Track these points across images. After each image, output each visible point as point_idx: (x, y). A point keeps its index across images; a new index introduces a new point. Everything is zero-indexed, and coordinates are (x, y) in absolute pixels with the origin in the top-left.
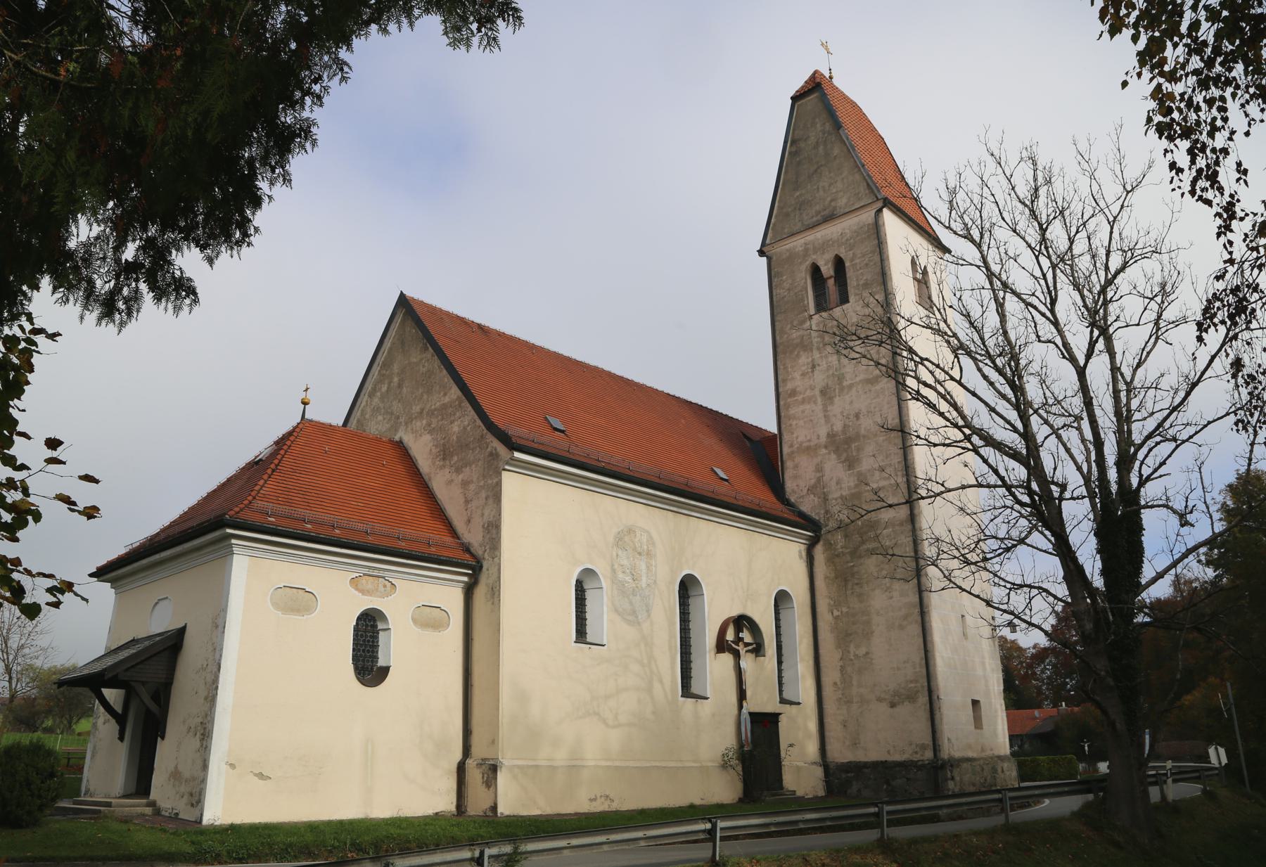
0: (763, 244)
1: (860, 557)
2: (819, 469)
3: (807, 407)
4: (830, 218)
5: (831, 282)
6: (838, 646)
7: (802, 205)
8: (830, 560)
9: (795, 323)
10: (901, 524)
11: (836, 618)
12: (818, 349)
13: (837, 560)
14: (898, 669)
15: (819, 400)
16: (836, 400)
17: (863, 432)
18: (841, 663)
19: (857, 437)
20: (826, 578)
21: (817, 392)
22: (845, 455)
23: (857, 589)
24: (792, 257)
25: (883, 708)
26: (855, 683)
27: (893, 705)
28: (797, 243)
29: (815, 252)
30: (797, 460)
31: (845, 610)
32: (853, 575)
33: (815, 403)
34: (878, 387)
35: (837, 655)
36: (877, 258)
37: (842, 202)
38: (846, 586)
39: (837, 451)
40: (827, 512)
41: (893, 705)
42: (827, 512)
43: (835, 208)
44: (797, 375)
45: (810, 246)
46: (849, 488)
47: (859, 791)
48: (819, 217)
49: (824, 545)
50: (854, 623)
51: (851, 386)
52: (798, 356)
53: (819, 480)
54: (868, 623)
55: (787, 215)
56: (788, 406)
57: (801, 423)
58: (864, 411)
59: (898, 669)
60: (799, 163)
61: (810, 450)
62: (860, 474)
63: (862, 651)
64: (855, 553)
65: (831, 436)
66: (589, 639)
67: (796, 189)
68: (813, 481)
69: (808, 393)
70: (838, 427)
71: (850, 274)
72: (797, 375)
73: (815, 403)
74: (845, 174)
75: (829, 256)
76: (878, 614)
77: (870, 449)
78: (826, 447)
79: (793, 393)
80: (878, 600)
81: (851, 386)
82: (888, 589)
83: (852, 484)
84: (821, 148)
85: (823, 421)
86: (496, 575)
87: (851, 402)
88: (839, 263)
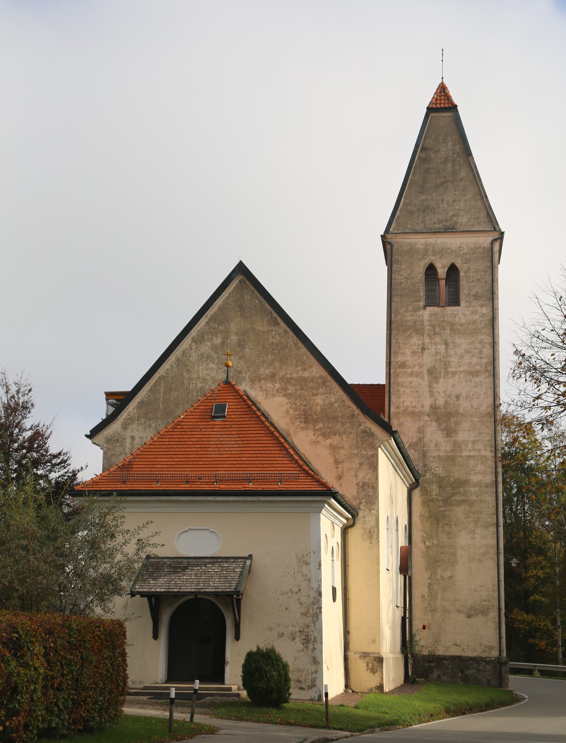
0: (387, 231)
1: (451, 505)
2: (421, 431)
3: (415, 380)
4: (450, 230)
5: (443, 283)
6: (428, 568)
7: (425, 209)
8: (426, 503)
9: (410, 308)
10: (487, 486)
11: (428, 547)
12: (429, 335)
13: (431, 504)
14: (475, 590)
15: (426, 377)
16: (441, 380)
17: (461, 410)
18: (429, 581)
19: (457, 413)
20: (421, 516)
21: (425, 370)
22: (444, 425)
23: (447, 528)
24: (412, 251)
25: (462, 618)
26: (439, 596)
27: (469, 616)
28: (420, 241)
29: (434, 255)
30: (401, 420)
31: (435, 542)
32: (444, 517)
33: (422, 378)
34: (477, 380)
35: (427, 575)
36: (489, 278)
37: (463, 220)
38: (438, 524)
39: (438, 420)
40: (425, 466)
41: (469, 616)
42: (425, 466)
43: (456, 223)
44: (408, 352)
45: (430, 248)
46: (446, 451)
47: (439, 676)
48: (440, 226)
49: (421, 490)
50: (442, 553)
51: (454, 373)
52: (410, 336)
53: (420, 439)
54: (454, 554)
55: (411, 213)
56: (397, 375)
57: (408, 391)
58: (464, 394)
59: (475, 590)
60: (427, 170)
61: (415, 415)
62: (455, 443)
63: (447, 574)
64: (446, 501)
65: (434, 408)
66: (382, 381)
67: (422, 193)
68: (415, 440)
69: (417, 369)
70: (441, 402)
71: (463, 283)
72: (408, 352)
73: (422, 378)
74: (468, 197)
75: (447, 262)
76: (462, 549)
77: (466, 425)
78: (429, 415)
79: (403, 365)
80: (463, 539)
81: (454, 373)
82: (472, 532)
83: (448, 449)
84: (450, 165)
85: (427, 394)
86: (373, 523)
87: (454, 386)
88: (453, 270)
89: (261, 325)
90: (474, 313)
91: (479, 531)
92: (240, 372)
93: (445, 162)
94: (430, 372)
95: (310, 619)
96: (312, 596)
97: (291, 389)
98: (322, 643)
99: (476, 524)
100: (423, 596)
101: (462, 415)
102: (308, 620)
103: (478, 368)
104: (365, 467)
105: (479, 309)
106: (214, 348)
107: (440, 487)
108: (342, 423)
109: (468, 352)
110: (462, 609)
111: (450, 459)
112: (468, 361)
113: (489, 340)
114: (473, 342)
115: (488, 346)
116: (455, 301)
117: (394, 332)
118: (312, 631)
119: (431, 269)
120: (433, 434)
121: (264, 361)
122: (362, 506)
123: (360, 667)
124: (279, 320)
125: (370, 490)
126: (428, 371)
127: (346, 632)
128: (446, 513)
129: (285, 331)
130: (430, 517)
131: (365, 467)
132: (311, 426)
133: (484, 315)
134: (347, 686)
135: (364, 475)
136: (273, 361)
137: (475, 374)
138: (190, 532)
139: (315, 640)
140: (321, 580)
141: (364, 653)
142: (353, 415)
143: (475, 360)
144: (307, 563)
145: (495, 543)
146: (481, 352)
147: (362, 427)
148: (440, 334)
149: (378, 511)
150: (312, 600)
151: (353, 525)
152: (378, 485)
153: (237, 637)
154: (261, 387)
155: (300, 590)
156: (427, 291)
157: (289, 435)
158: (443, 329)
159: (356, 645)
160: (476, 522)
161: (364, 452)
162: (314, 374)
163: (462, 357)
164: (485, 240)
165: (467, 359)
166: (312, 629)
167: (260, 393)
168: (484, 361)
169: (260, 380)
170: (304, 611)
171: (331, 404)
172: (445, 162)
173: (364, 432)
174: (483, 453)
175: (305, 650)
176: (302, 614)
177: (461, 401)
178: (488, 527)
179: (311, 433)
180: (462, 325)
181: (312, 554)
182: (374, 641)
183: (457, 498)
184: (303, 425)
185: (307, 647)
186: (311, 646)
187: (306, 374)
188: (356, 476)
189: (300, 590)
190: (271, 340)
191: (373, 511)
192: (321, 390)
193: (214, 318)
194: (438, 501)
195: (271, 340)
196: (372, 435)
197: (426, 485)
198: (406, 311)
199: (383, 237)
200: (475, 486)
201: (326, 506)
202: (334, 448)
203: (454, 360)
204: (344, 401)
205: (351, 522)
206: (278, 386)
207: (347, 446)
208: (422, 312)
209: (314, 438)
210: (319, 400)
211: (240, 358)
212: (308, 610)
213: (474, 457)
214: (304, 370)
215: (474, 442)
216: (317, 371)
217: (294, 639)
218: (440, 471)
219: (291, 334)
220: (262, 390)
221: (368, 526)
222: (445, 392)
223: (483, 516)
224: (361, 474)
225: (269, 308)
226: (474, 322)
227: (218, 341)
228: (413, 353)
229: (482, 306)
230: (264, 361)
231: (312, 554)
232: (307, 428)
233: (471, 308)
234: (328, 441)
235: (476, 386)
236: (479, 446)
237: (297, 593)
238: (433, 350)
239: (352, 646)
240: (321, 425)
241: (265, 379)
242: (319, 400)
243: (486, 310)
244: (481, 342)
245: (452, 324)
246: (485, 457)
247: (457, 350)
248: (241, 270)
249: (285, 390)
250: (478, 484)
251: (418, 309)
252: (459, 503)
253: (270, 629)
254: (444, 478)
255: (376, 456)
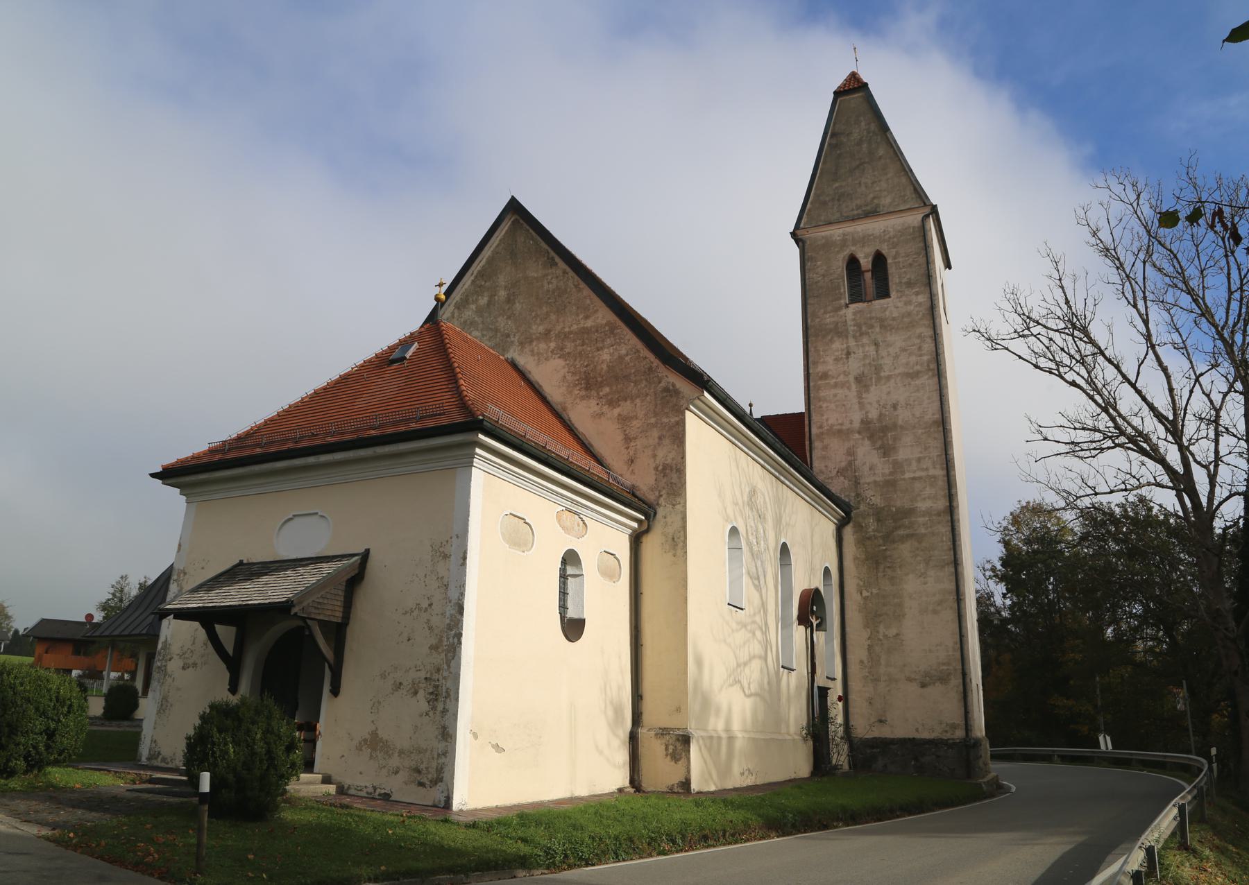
0: (797, 227)
1: (894, 542)
2: (851, 453)
3: (839, 391)
5: (868, 276)
6: (866, 626)
8: (862, 542)
9: (829, 308)
10: (939, 514)
11: (866, 598)
12: (854, 337)
13: (868, 543)
14: (930, 651)
15: (854, 387)
16: (872, 388)
17: (900, 422)
19: (895, 426)
20: (856, 558)
21: (851, 379)
22: (879, 443)
23: (889, 572)
24: (828, 245)
26: (883, 662)
27: (923, 685)
28: (836, 232)
29: (854, 244)
30: (826, 442)
31: (875, 591)
32: (885, 558)
33: (849, 388)
34: (918, 382)
36: (922, 260)
37: (886, 201)
40: (858, 495)
41: (923, 685)
42: (858, 495)
43: (878, 206)
45: (849, 237)
46: (883, 475)
48: (860, 211)
49: (854, 526)
50: (884, 605)
51: (889, 378)
52: (831, 341)
53: (850, 463)
55: (825, 203)
56: (818, 388)
57: (832, 406)
59: (930, 651)
61: (842, 433)
63: (892, 632)
64: (888, 538)
65: (866, 423)
67: (835, 180)
68: (843, 464)
69: (842, 378)
70: (874, 414)
71: (892, 270)
72: (830, 360)
73: (849, 388)
74: (890, 175)
77: (908, 439)
78: (859, 433)
79: (825, 376)
80: (911, 585)
81: (889, 378)
83: (887, 471)
84: (865, 146)
85: (856, 407)
87: (889, 393)
88: (879, 260)
89: (534, 270)
90: (908, 303)
91: (931, 573)
92: (508, 336)
93: (859, 143)
94: (859, 379)
95: (443, 655)
96: (448, 614)
97: (569, 347)
98: (457, 699)
99: (927, 564)
100: (862, 662)
101: (902, 427)
102: (438, 659)
103: (918, 368)
104: (666, 442)
105: (914, 297)
106: (480, 311)
107: (879, 520)
108: (635, 382)
109: (904, 350)
110: (913, 676)
111: (890, 485)
112: (904, 361)
113: (928, 332)
114: (909, 338)
115: (929, 340)
116: (883, 292)
117: (811, 339)
118: (445, 678)
119: (853, 263)
120: (867, 455)
121: (537, 316)
122: (662, 501)
123: (653, 749)
124: (558, 259)
125: (673, 476)
126: (856, 379)
127: (637, 697)
128: (888, 553)
129: (565, 272)
130: (867, 559)
131: (666, 442)
132: (594, 393)
133: (920, 304)
134: (635, 781)
135: (665, 454)
136: (548, 314)
137: (916, 375)
138: (297, 519)
139: (448, 696)
140: (464, 585)
141: (664, 729)
142: (650, 369)
143: (913, 359)
144: (446, 557)
145: (954, 587)
146: (920, 348)
147: (663, 384)
148: (867, 333)
149: (685, 506)
150: (448, 621)
151: (647, 531)
152: (685, 467)
153: (335, 691)
154: (532, 351)
155: (430, 605)
156: (850, 287)
157: (565, 409)
158: (872, 327)
159: (655, 715)
160: (927, 562)
161: (665, 420)
162: (599, 321)
163: (897, 357)
164: (914, 219)
165: (903, 359)
166: (445, 674)
167: (531, 359)
168: (925, 358)
169: (531, 342)
170: (434, 641)
171: (621, 358)
172: (859, 143)
173: (666, 390)
174: (932, 472)
175: (431, 713)
176: (431, 648)
177: (900, 411)
178: (943, 567)
179: (593, 402)
180: (894, 319)
181: (454, 538)
182: (678, 710)
183: (901, 532)
184: (583, 393)
185: (434, 708)
186: (440, 706)
187: (589, 323)
188: (654, 456)
189: (430, 605)
190: (546, 286)
191: (678, 507)
192: (608, 341)
193: (481, 274)
194: (876, 538)
195: (546, 286)
196: (676, 392)
197: (860, 520)
198: (825, 313)
199: (794, 235)
200: (924, 516)
201: (478, 451)
202: (624, 420)
203: (887, 362)
204: (638, 351)
205: (645, 527)
206: (553, 345)
207: (641, 414)
208: (844, 311)
209: (597, 408)
210: (605, 356)
211: (509, 318)
212: (441, 640)
213: (920, 478)
214: (587, 317)
215: (919, 460)
216: (604, 315)
217: (416, 693)
218: (877, 501)
219: (571, 273)
220: (533, 355)
221: (670, 530)
222: (878, 402)
223: (936, 552)
224: (661, 453)
225: (544, 245)
226: (909, 314)
227: (483, 301)
228: (837, 360)
229: (917, 294)
230: (537, 316)
231: (454, 538)
232: (588, 397)
233: (904, 299)
234: (617, 411)
235: (918, 390)
236: (927, 463)
237: (426, 610)
238: (860, 353)
239: (647, 718)
240: (607, 390)
241: (538, 339)
242: (605, 356)
243: (923, 298)
244: (920, 336)
245: (882, 321)
246: (934, 477)
247: (890, 350)
248: (514, 208)
249: (562, 349)
250: (928, 513)
251: (840, 308)
252: (903, 539)
253: (383, 676)
254: (883, 508)
255: (682, 424)
